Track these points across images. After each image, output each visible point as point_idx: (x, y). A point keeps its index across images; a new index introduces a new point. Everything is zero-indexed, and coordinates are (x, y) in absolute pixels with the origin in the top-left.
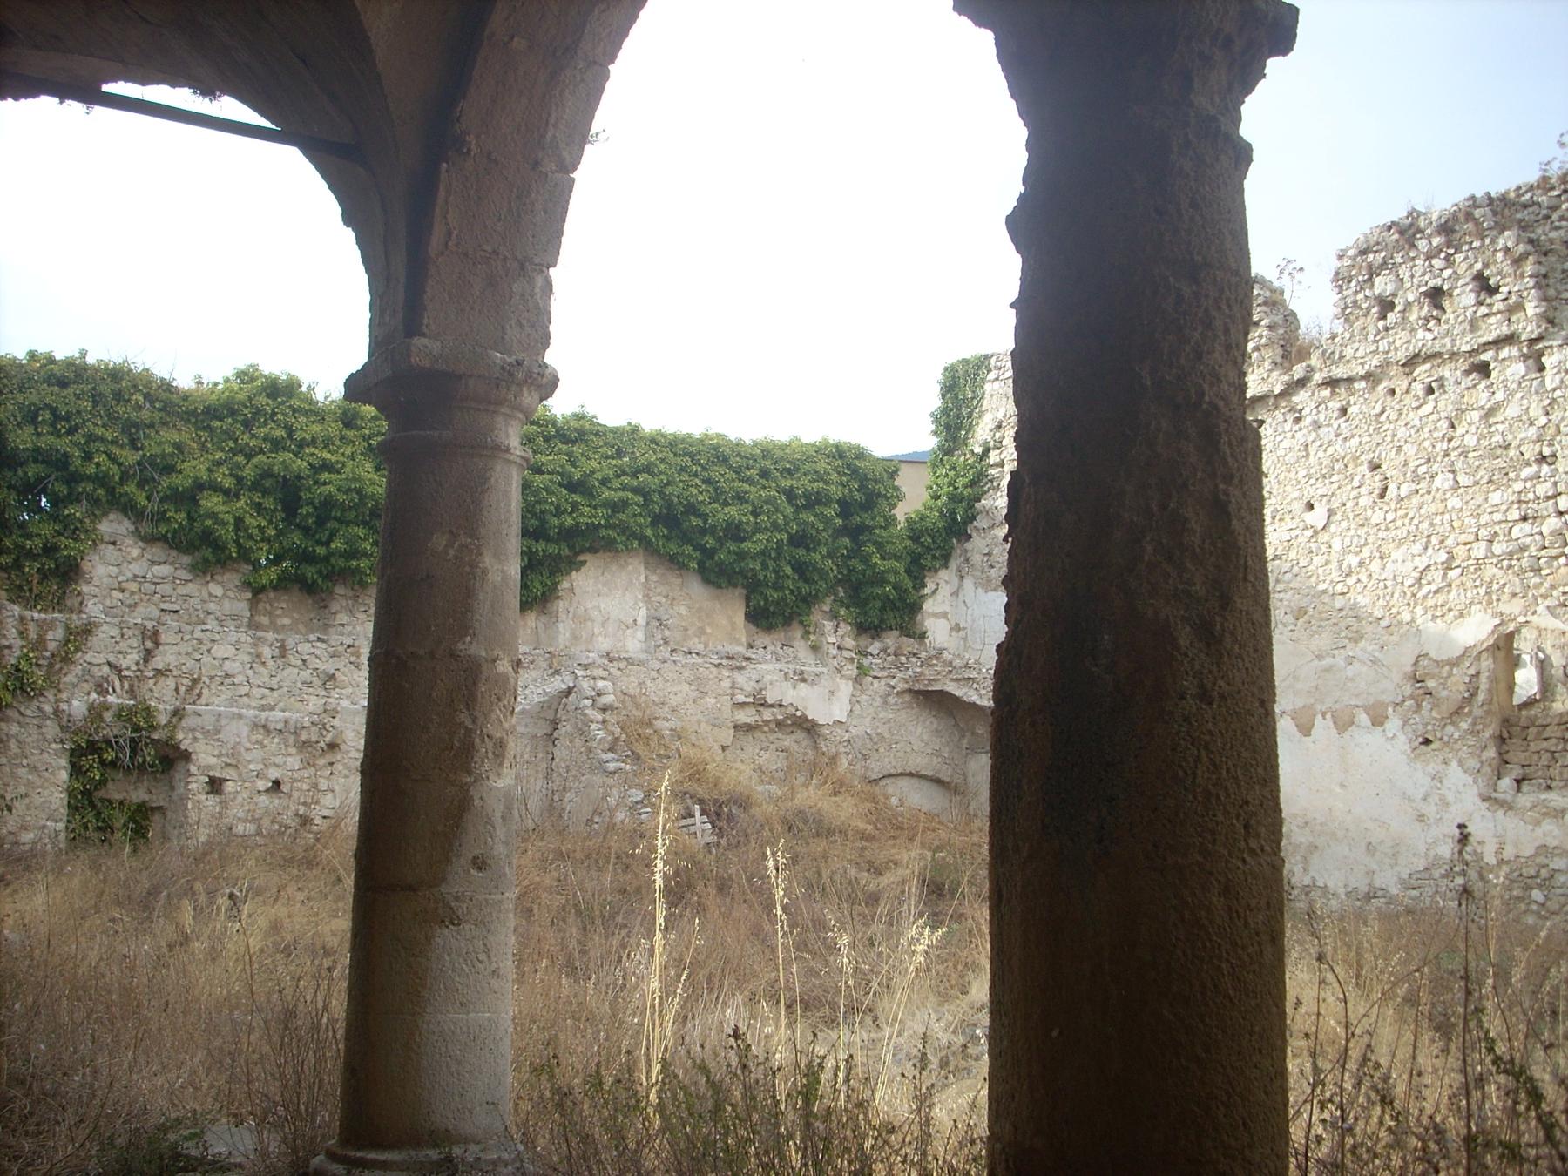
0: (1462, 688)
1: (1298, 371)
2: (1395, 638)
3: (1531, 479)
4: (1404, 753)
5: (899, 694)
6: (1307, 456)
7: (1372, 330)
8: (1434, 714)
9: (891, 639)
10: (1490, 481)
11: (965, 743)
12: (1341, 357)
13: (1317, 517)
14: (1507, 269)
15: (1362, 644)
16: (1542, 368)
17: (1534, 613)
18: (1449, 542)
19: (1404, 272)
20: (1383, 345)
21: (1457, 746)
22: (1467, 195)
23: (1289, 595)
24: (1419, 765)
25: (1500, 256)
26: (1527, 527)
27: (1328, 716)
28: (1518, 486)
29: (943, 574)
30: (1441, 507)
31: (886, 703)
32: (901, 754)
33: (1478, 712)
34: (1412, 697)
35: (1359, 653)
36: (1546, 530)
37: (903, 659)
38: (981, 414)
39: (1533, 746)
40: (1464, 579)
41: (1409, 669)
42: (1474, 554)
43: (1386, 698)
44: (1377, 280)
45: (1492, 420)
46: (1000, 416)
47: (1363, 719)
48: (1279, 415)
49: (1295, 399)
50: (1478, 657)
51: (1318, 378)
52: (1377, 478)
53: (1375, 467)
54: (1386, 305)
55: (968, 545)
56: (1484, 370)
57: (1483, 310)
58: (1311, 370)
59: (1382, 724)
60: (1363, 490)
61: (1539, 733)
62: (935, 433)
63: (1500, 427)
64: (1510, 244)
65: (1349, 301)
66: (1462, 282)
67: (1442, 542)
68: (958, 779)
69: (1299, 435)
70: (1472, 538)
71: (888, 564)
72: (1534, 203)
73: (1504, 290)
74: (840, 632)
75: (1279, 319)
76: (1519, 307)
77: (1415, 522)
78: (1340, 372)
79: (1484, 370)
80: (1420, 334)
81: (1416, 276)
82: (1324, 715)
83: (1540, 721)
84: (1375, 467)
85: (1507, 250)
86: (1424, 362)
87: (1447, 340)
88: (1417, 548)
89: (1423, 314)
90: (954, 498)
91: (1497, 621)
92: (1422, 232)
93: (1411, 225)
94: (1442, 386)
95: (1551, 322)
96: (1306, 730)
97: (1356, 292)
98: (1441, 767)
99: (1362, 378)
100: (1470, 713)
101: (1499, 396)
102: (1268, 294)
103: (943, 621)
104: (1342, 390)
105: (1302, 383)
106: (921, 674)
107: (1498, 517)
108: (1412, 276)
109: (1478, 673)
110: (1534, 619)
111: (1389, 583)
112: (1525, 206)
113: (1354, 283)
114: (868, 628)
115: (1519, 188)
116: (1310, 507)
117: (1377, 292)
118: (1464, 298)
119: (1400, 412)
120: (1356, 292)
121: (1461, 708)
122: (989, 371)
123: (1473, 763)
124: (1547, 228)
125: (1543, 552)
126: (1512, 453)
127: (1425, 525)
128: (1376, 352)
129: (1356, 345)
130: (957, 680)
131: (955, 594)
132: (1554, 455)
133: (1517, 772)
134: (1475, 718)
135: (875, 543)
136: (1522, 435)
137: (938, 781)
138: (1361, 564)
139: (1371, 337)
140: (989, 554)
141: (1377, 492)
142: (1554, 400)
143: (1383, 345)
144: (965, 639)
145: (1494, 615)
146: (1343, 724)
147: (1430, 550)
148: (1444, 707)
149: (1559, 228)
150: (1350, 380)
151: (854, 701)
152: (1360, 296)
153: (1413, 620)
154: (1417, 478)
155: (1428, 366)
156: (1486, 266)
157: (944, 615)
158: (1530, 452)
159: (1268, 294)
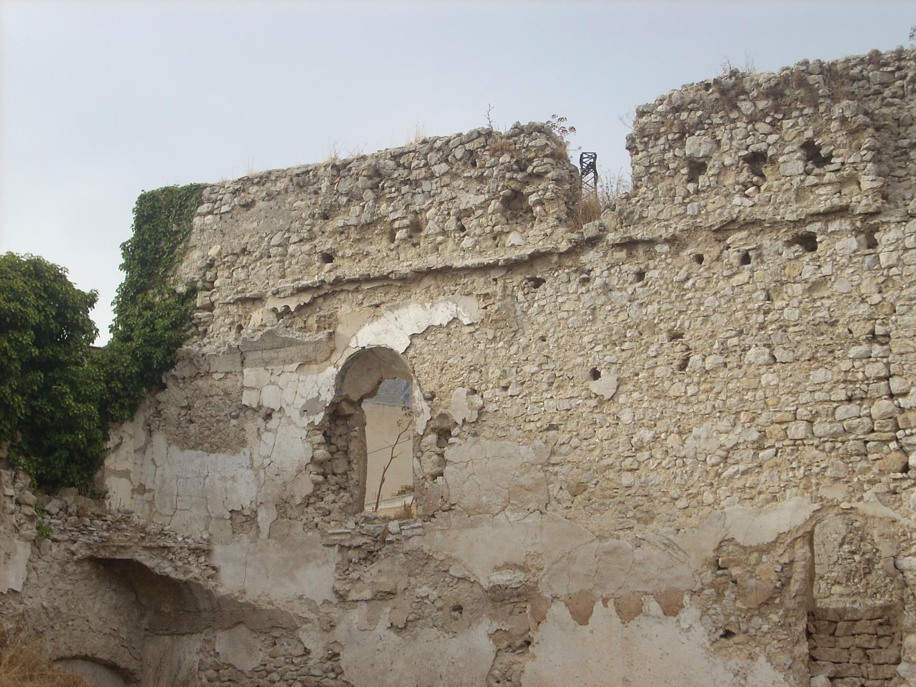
0: (773, 577)
1: (590, 229)
2: (694, 521)
3: (860, 359)
4: (702, 646)
5: (79, 562)
6: (593, 321)
7: (680, 191)
8: (739, 604)
9: (70, 497)
10: (812, 358)
11: (144, 623)
12: (642, 218)
13: (605, 385)
14: (841, 139)
15: (654, 525)
16: (873, 244)
17: (860, 499)
18: (762, 420)
19: (722, 135)
20: (692, 209)
21: (764, 640)
22: (801, 59)
23: (566, 469)
24: (718, 660)
25: (834, 125)
26: (853, 408)
27: (611, 603)
28: (845, 365)
29: (128, 427)
30: (754, 383)
31: (64, 571)
32: (77, 633)
33: (790, 603)
34: (711, 585)
35: (650, 536)
36: (875, 411)
37: (87, 521)
38: (186, 250)
39: (843, 642)
40: (778, 460)
41: (711, 554)
42: (791, 433)
43: (682, 585)
44: (689, 141)
45: (816, 295)
46: (213, 252)
47: (654, 607)
48: (562, 274)
49: (584, 259)
50: (792, 545)
51: (611, 237)
52: (678, 348)
53: (675, 336)
54: (697, 167)
55: (161, 396)
56: (809, 243)
57: (811, 180)
58: (603, 229)
59: (675, 614)
60: (661, 360)
61: (848, 628)
62: (123, 267)
63: (827, 302)
64: (848, 114)
65: (655, 160)
66: (788, 149)
67: (753, 420)
68: (133, 666)
69: (586, 297)
70: (790, 417)
71: (83, 408)
72: (863, 78)
73: (837, 161)
74: (19, 484)
75: (565, 173)
76: (853, 179)
77: (722, 396)
78: (639, 233)
79: (809, 243)
80: (737, 200)
81: (734, 140)
82: (605, 601)
83: (850, 616)
84: (675, 336)
85: (843, 120)
86: (741, 228)
87: (769, 209)
88: (724, 424)
89: (742, 179)
90: (153, 342)
91: (817, 506)
92: (746, 93)
93: (734, 86)
94: (760, 255)
95: (885, 197)
96: (582, 617)
97: (664, 151)
98: (744, 663)
99: (667, 241)
100: (782, 603)
101: (826, 270)
102: (554, 146)
103: (124, 481)
104: (641, 250)
105: (592, 242)
106: (108, 539)
107: (819, 396)
108: (731, 139)
109: (792, 562)
110: (860, 505)
111: (689, 461)
112: (854, 80)
113: (662, 140)
114: (47, 484)
115: (847, 61)
116: (596, 375)
117: (688, 153)
118: (792, 164)
119: (708, 280)
120: (664, 151)
121: (772, 598)
122: (201, 203)
123: (784, 659)
124: (878, 103)
125: (872, 436)
126: (840, 329)
127: (734, 400)
128: (682, 216)
129: (661, 206)
130: (150, 549)
131: (142, 450)
132: (887, 335)
133: (830, 669)
134: (788, 610)
135: (71, 383)
136: (853, 312)
137: (112, 667)
138: (655, 439)
139: (678, 199)
140: (189, 408)
141: (677, 363)
142: (889, 278)
143: (692, 209)
144: (151, 503)
145: (814, 499)
146: (629, 611)
147: (739, 429)
148: (752, 597)
149: (893, 105)
150: (652, 242)
151: (31, 567)
152: (669, 155)
153: (717, 502)
154: (724, 350)
155: (744, 234)
156: (817, 134)
157: (126, 474)
158: (861, 330)
159: (554, 146)
